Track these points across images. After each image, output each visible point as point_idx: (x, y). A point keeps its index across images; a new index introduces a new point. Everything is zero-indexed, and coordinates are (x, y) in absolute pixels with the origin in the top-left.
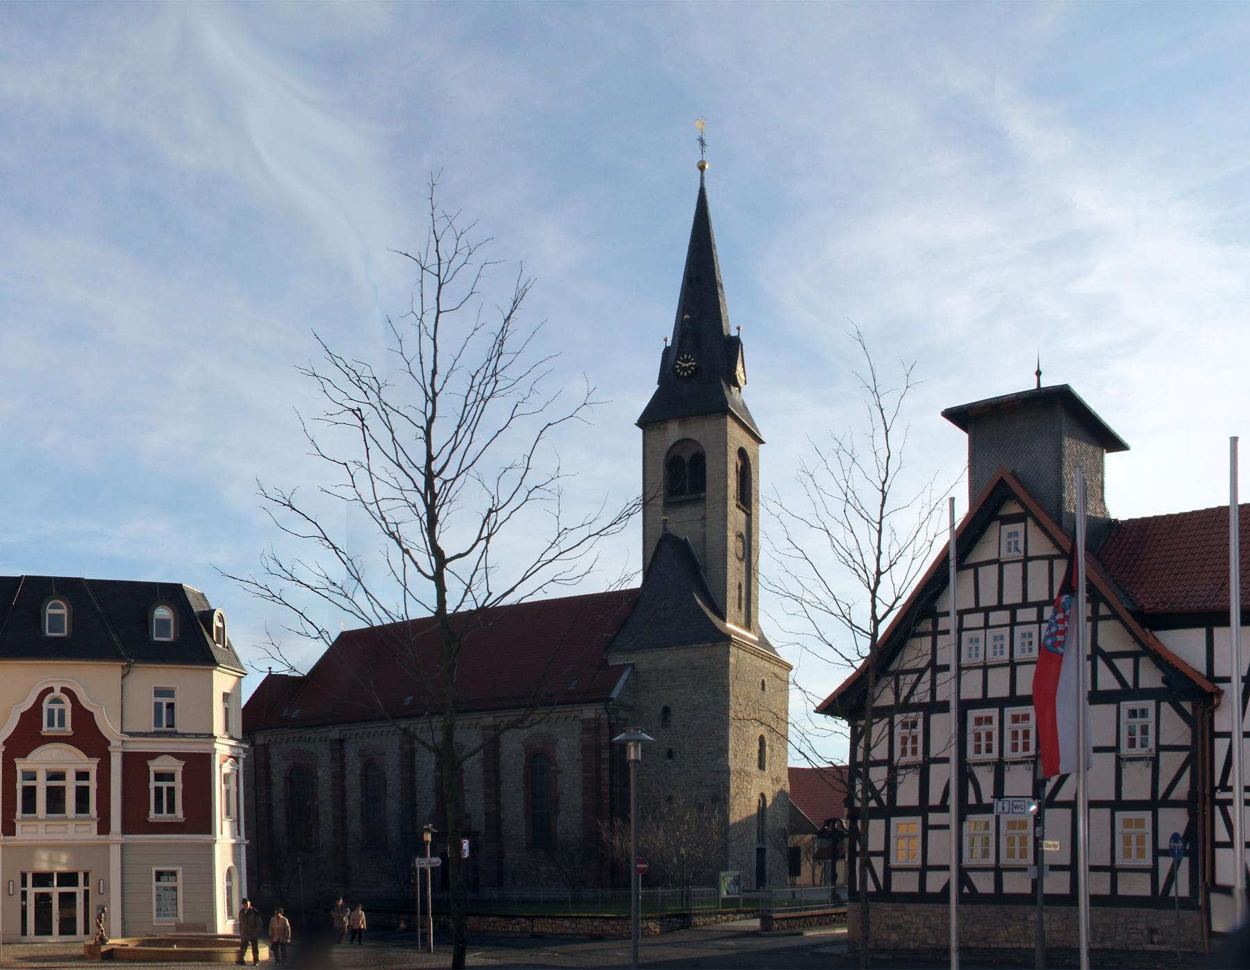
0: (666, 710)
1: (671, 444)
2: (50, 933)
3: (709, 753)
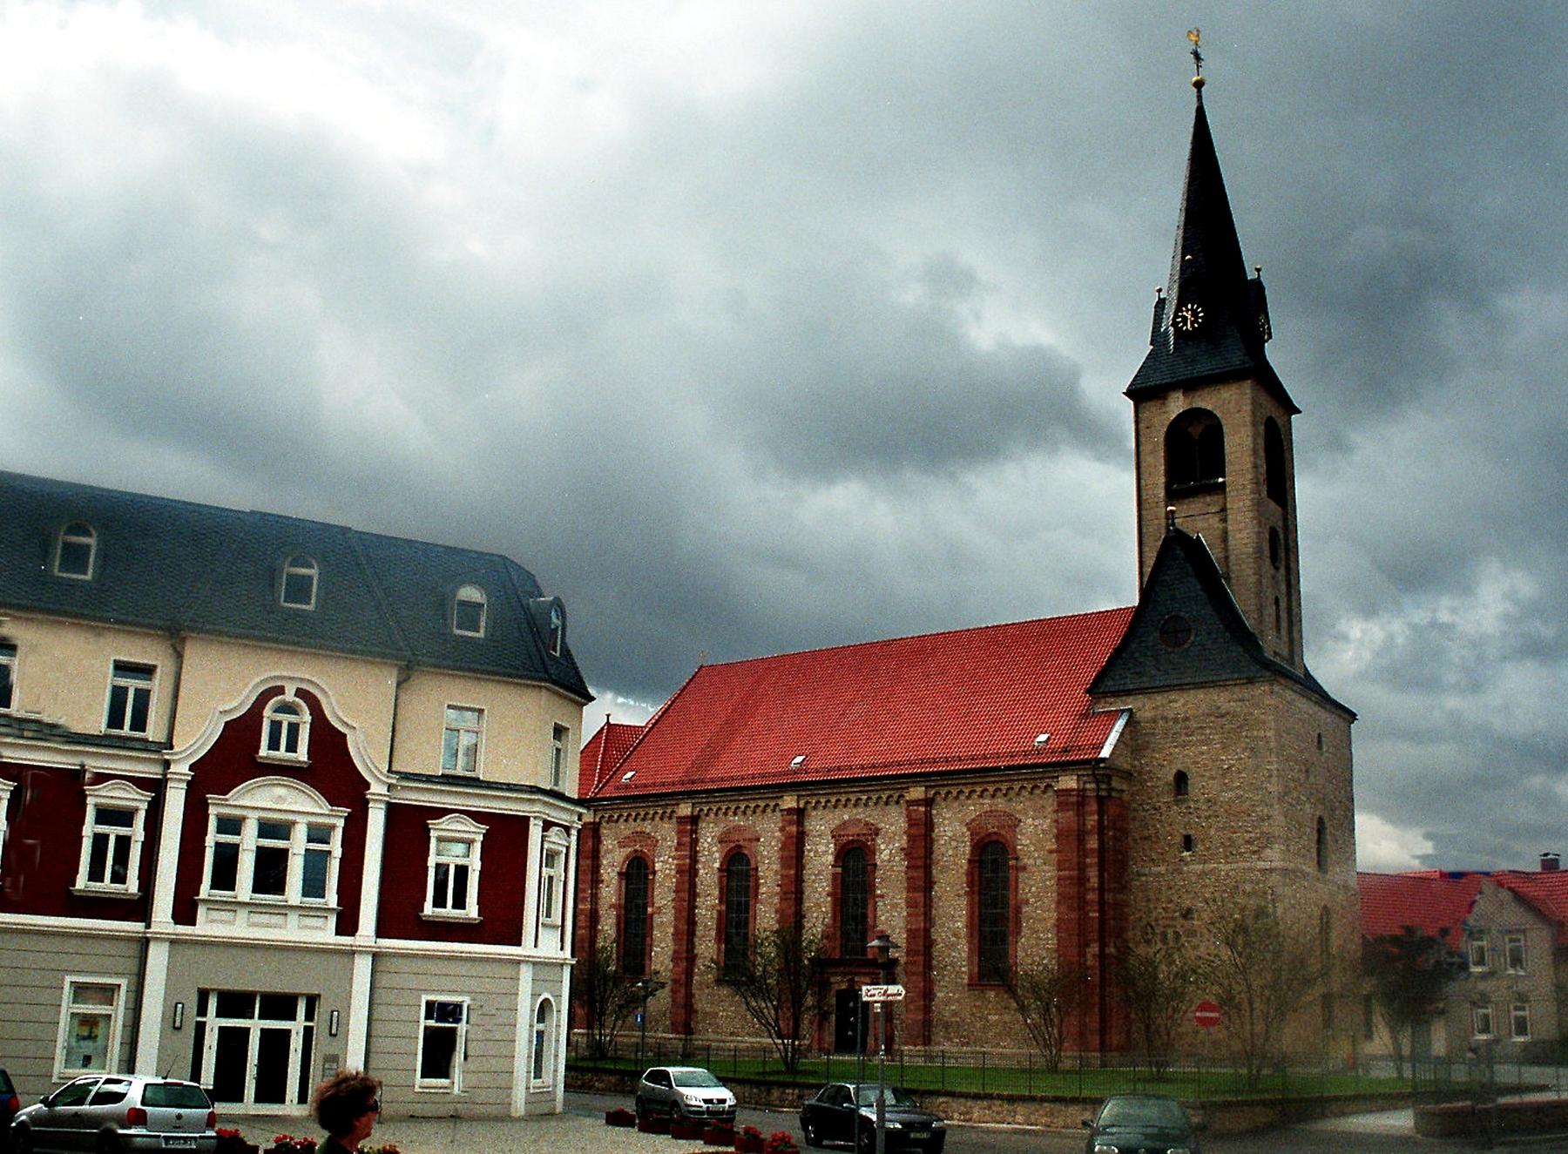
0: (1181, 779)
2: (260, 835)
3: (1248, 842)
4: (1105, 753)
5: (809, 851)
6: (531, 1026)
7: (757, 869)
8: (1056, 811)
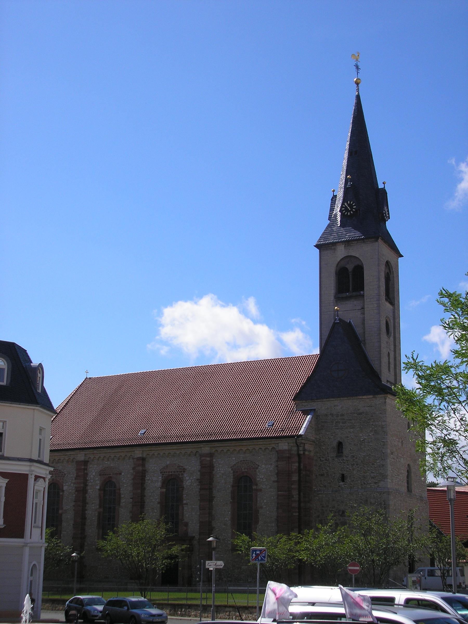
0: (340, 444)
1: (339, 259)
4: (301, 432)
5: (148, 480)
6: (28, 578)
7: (120, 489)
8: (277, 461)
